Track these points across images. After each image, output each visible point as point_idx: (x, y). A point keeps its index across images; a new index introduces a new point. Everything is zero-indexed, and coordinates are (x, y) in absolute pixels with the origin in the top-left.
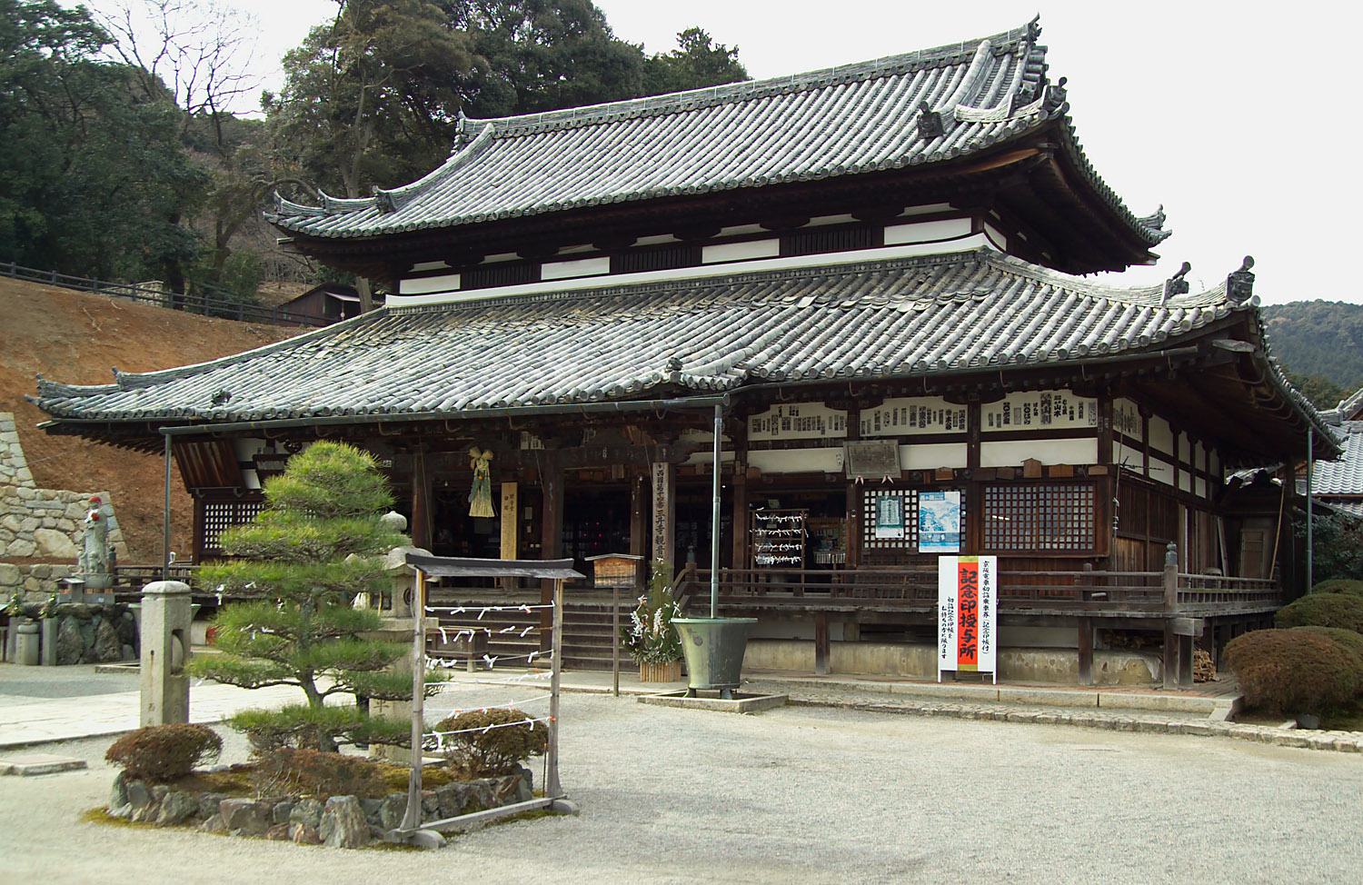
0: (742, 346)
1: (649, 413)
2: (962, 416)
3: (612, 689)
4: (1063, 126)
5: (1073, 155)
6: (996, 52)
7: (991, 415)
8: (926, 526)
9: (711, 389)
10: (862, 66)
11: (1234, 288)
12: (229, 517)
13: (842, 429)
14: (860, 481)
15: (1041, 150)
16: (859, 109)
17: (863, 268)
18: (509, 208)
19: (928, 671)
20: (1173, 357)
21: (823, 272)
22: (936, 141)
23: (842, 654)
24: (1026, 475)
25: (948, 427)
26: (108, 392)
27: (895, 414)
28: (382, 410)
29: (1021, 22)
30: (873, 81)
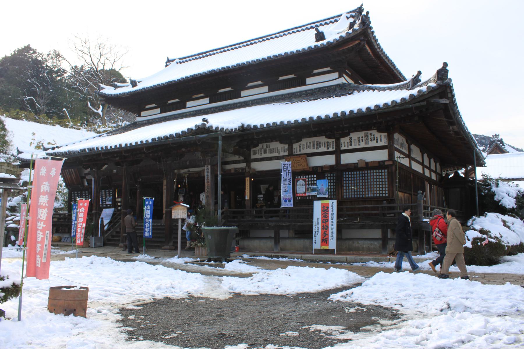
2: (333, 144)
7: (344, 143)
11: (440, 76)
15: (361, 40)
19: (308, 249)
20: (417, 108)
24: (359, 166)
25: (328, 149)
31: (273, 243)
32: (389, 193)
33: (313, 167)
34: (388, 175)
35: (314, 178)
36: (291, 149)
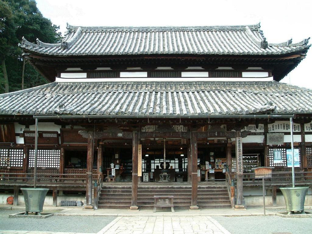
2: (299, 127)
3: (263, 213)
7: (307, 127)
8: (289, 159)
12: (6, 154)
13: (262, 130)
14: (271, 146)
17: (182, 83)
21: (225, 83)
27: (279, 126)
33: (286, 143)
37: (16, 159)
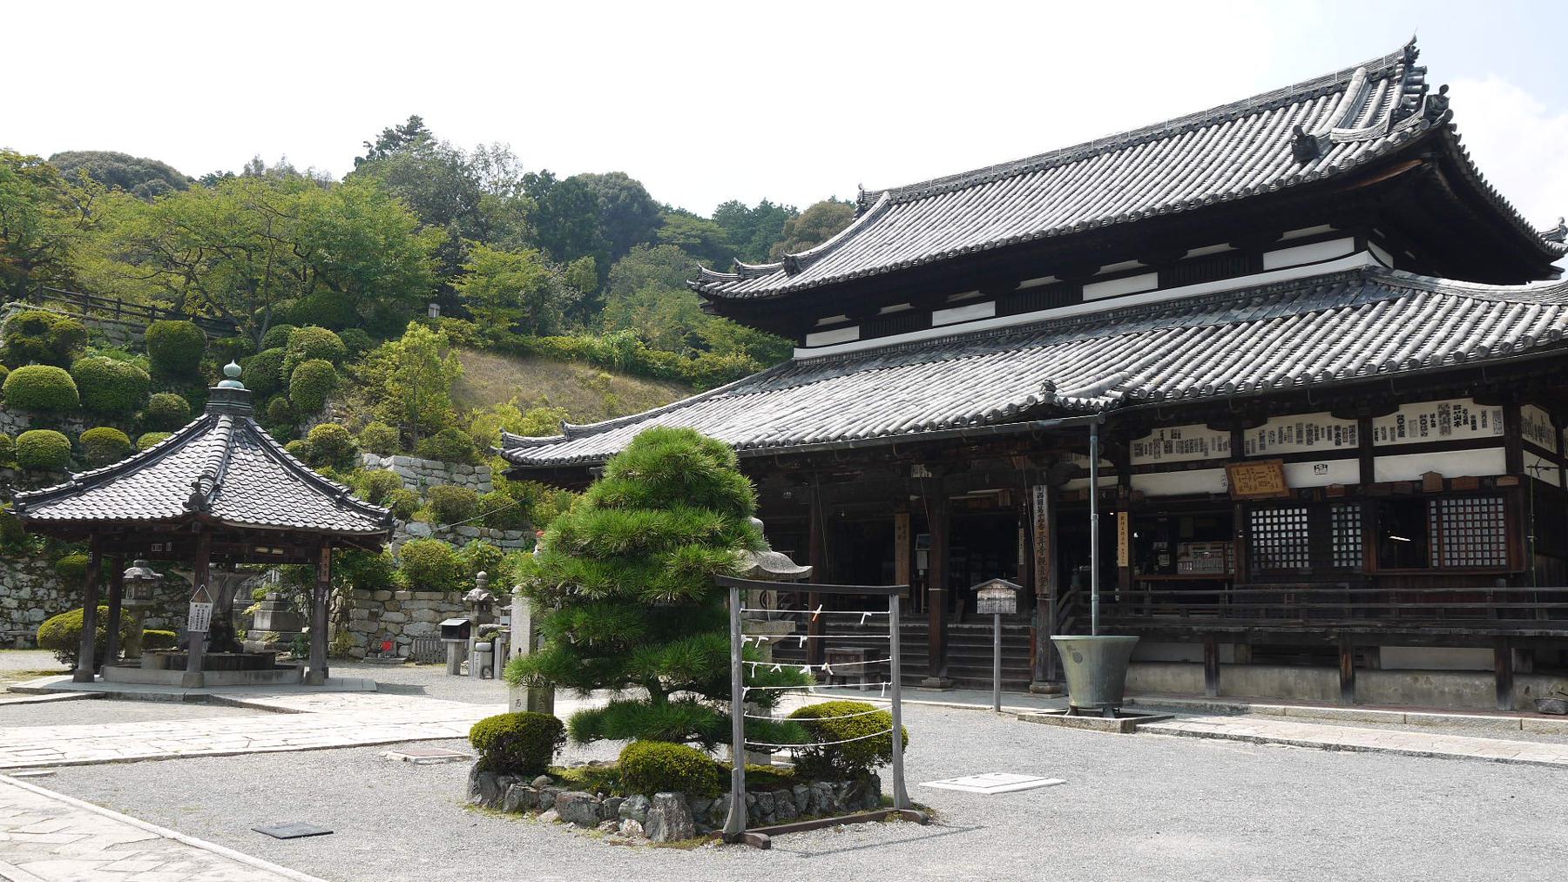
0: (1119, 370)
1: (1026, 435)
4: (1446, 134)
5: (1460, 163)
6: (1372, 80)
9: (1088, 409)
10: (1234, 105)
15: (1424, 161)
16: (1232, 144)
18: (900, 261)
22: (1310, 165)
23: (1233, 677)
25: (1338, 443)
26: (556, 442)
28: (777, 443)
29: (1395, 45)
30: (1246, 118)
31: (1200, 675)
32: (1508, 558)
34: (1505, 512)
35: (1301, 515)
36: (1238, 444)
37: (1458, 529)
